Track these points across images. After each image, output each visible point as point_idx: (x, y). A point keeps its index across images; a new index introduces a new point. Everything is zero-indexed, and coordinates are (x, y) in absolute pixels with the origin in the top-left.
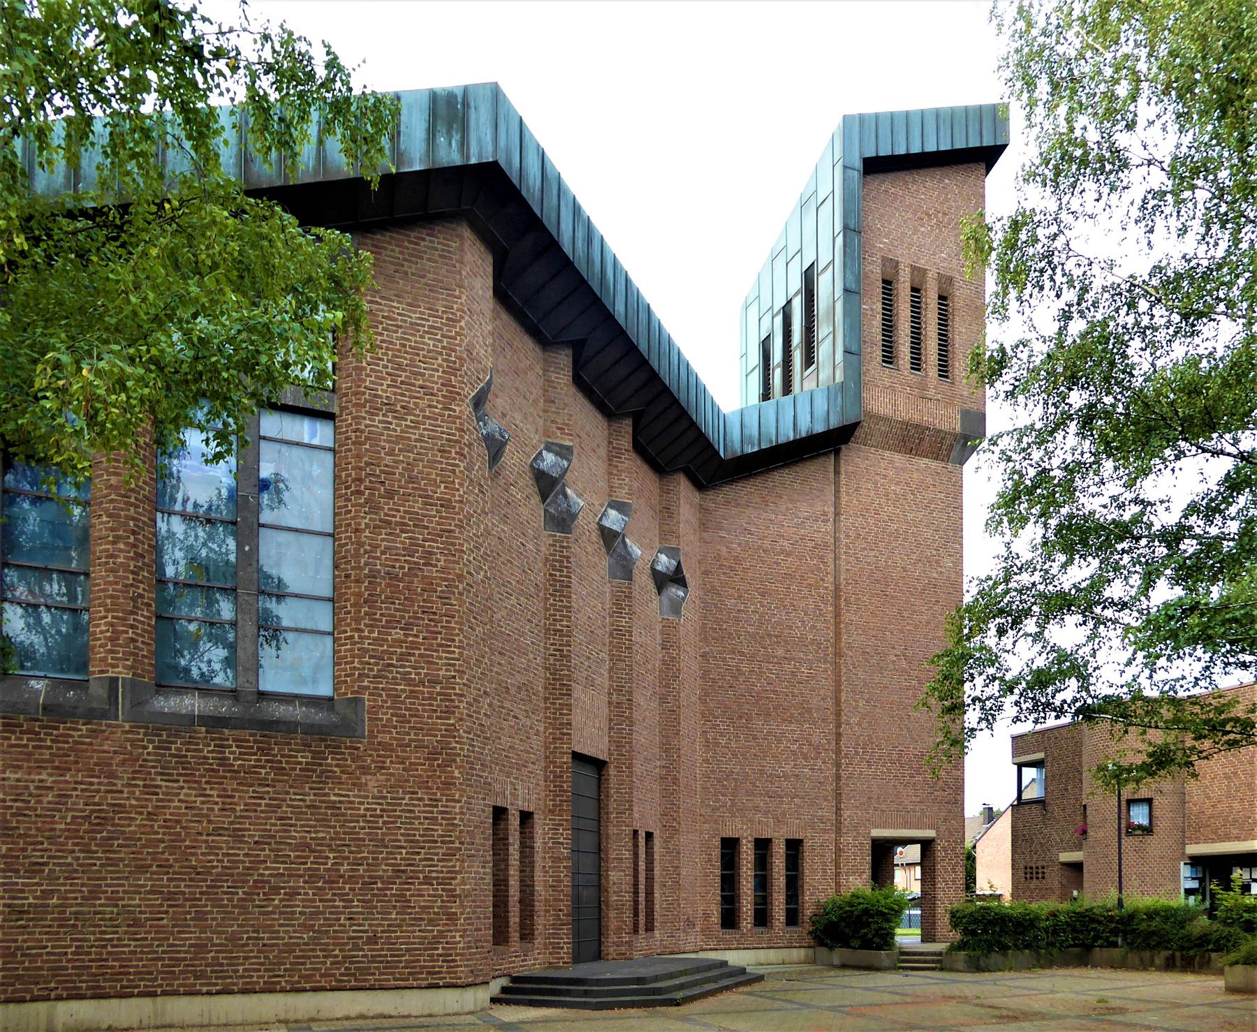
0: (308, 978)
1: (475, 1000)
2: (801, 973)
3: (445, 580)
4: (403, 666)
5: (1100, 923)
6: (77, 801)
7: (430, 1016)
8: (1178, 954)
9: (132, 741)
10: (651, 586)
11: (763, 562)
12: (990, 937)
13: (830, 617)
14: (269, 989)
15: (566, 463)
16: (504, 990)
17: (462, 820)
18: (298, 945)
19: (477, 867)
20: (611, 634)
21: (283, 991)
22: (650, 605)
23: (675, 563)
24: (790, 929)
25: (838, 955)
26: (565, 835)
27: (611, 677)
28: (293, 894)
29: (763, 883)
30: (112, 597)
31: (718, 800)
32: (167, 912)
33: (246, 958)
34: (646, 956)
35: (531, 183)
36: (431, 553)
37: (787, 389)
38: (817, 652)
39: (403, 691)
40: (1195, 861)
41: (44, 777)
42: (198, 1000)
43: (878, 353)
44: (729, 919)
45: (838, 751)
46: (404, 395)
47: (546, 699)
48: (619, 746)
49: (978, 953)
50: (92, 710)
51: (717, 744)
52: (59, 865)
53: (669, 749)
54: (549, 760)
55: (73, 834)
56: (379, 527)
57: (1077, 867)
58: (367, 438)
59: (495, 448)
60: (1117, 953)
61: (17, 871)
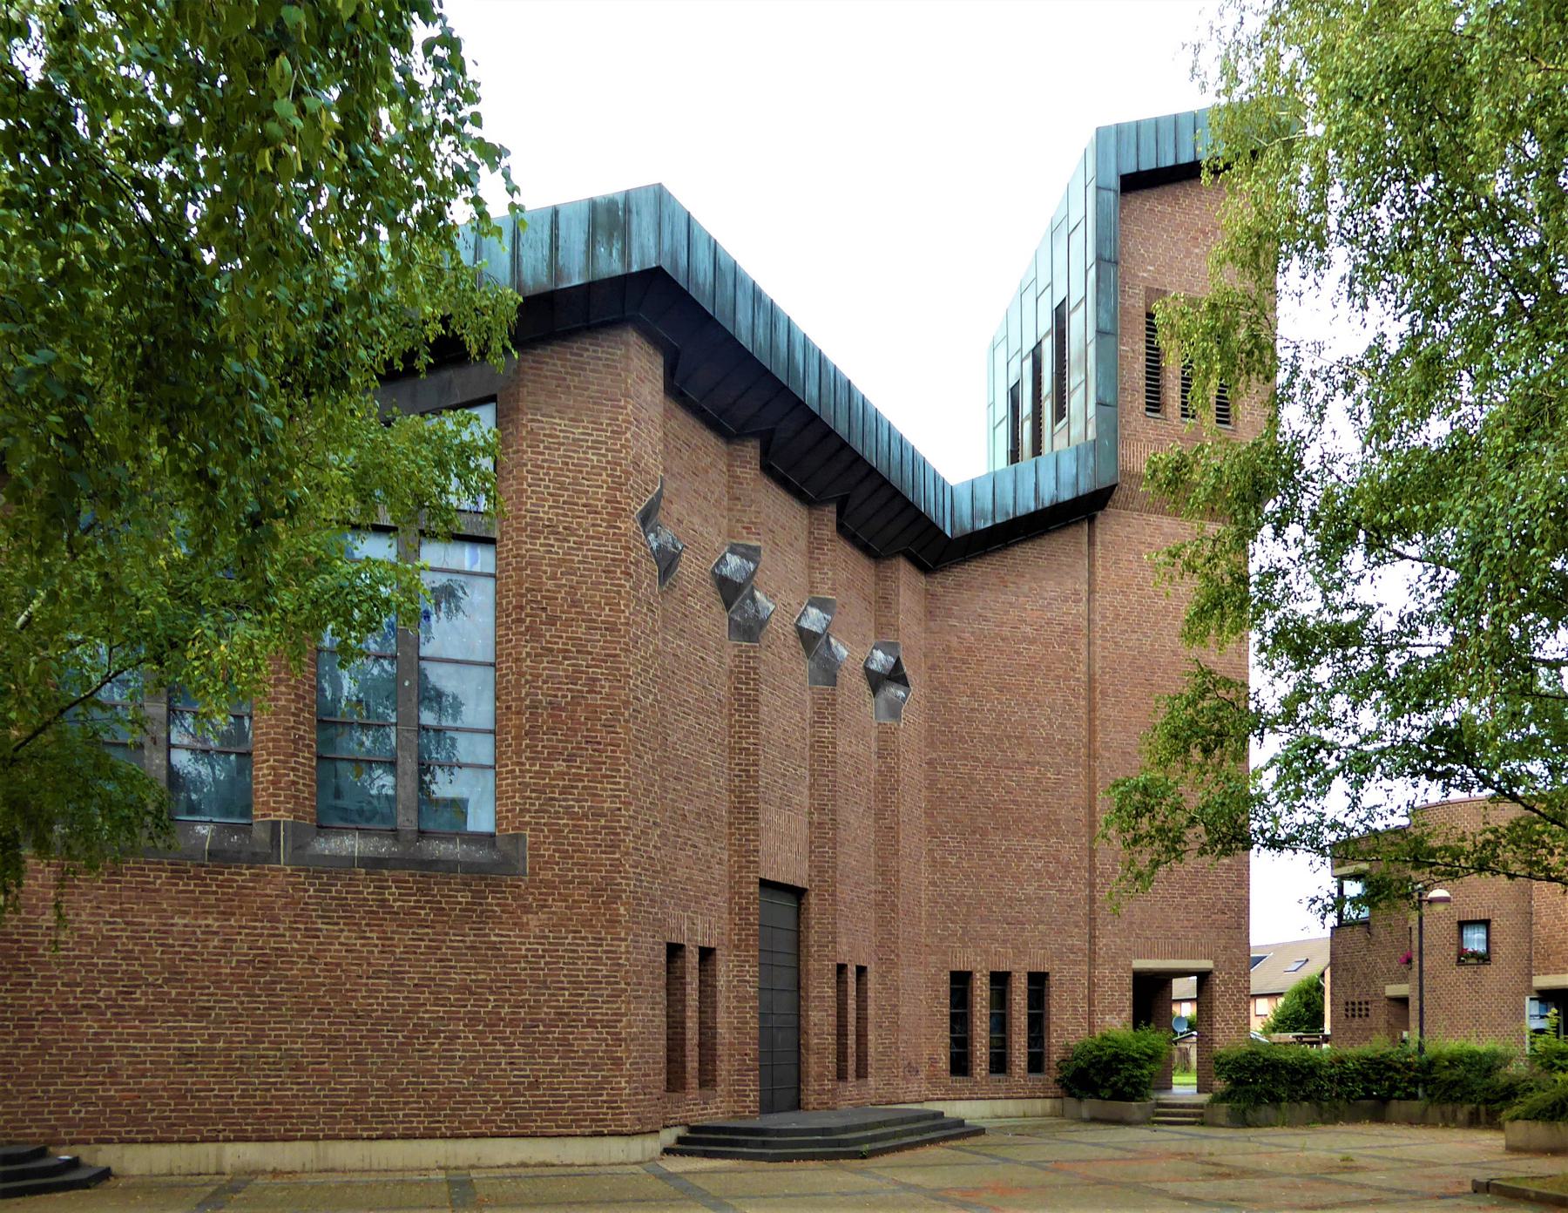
0: (468, 1124)
1: (643, 1150)
2: (1039, 1127)
3: (610, 707)
4: (565, 800)
5: (1397, 1071)
6: (241, 946)
7: (595, 1165)
8: (1482, 1108)
9: (293, 884)
10: (865, 687)
11: (1001, 652)
12: (1260, 1088)
13: (1082, 712)
14: (429, 1135)
15: (752, 566)
16: (680, 1140)
17: (628, 959)
18: (458, 1090)
19: (645, 1009)
20: (812, 747)
21: (443, 1137)
22: (862, 708)
23: (893, 660)
24: (1032, 1076)
25: (1088, 1107)
26: (751, 972)
27: (811, 795)
28: (453, 1038)
29: (1000, 1023)
30: (273, 740)
31: (946, 929)
32: (328, 1056)
33: (406, 1103)
34: (856, 1106)
35: (701, 280)
36: (595, 680)
37: (1037, 450)
38: (1066, 754)
39: (566, 825)
40: (1547, 997)
41: (210, 922)
42: (359, 1145)
43: (1141, 401)
44: (960, 1064)
45: (1092, 869)
46: (566, 515)
47: (731, 824)
48: (821, 871)
49: (1243, 1105)
50: (254, 854)
51: (945, 864)
52: (225, 1009)
53: (886, 872)
54: (734, 892)
55: (238, 978)
56: (541, 655)
57: (1403, 1001)
58: (528, 564)
59: (667, 562)
60: (1415, 1106)
61: (185, 1015)
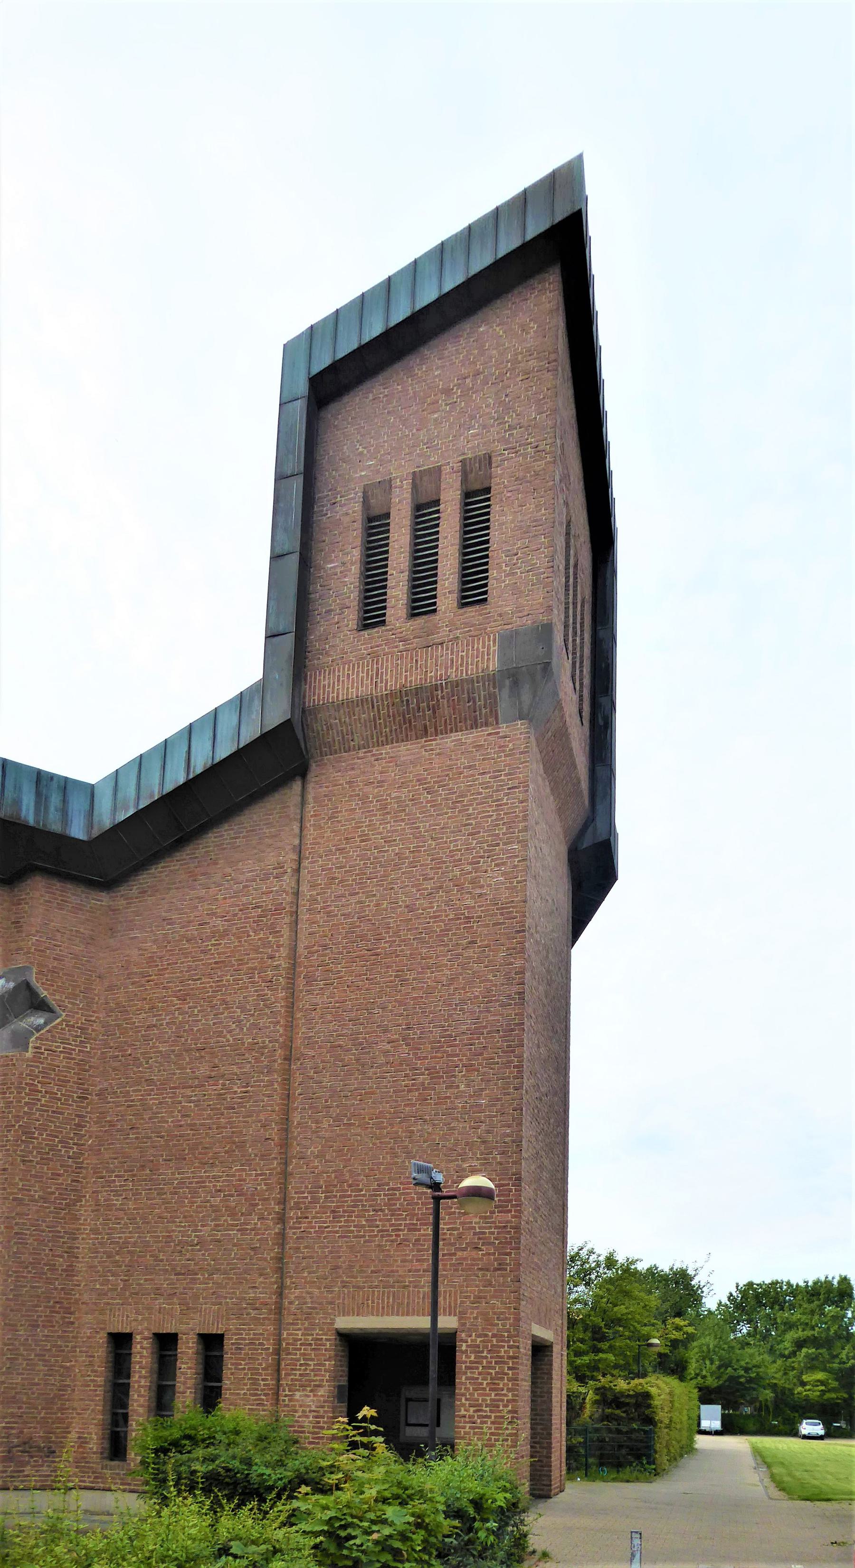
13: (280, 1007)
51: (109, 1207)
